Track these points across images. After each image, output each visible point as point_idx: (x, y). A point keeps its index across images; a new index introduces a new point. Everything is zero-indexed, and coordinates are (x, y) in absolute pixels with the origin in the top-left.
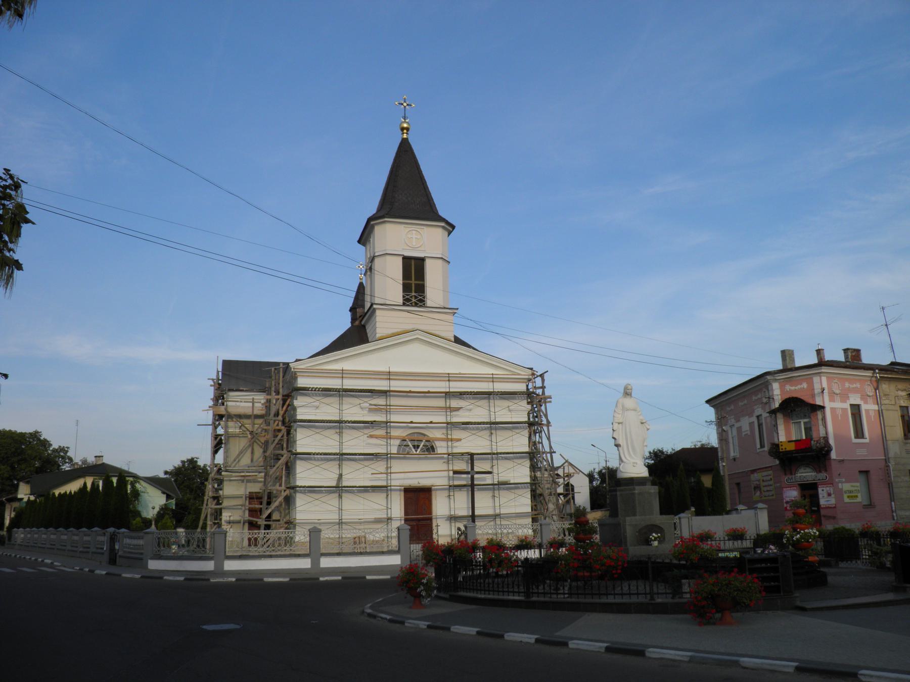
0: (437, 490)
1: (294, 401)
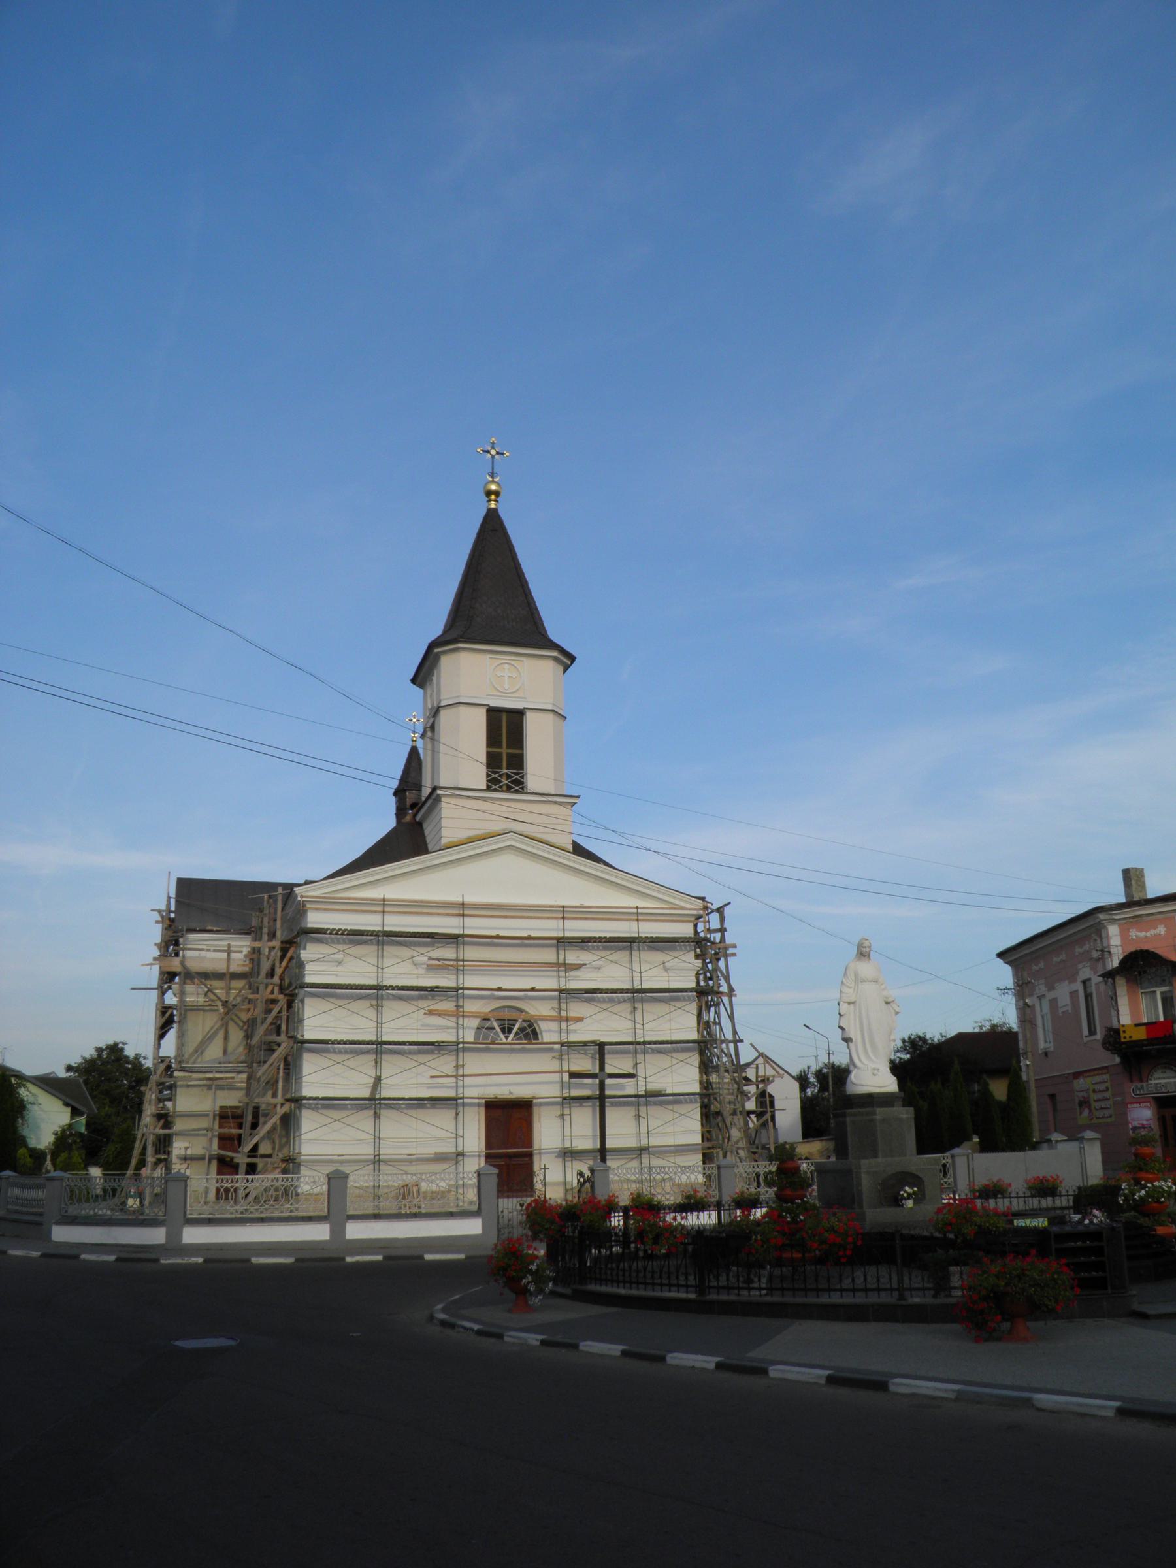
0: (541, 1104)
1: (301, 951)
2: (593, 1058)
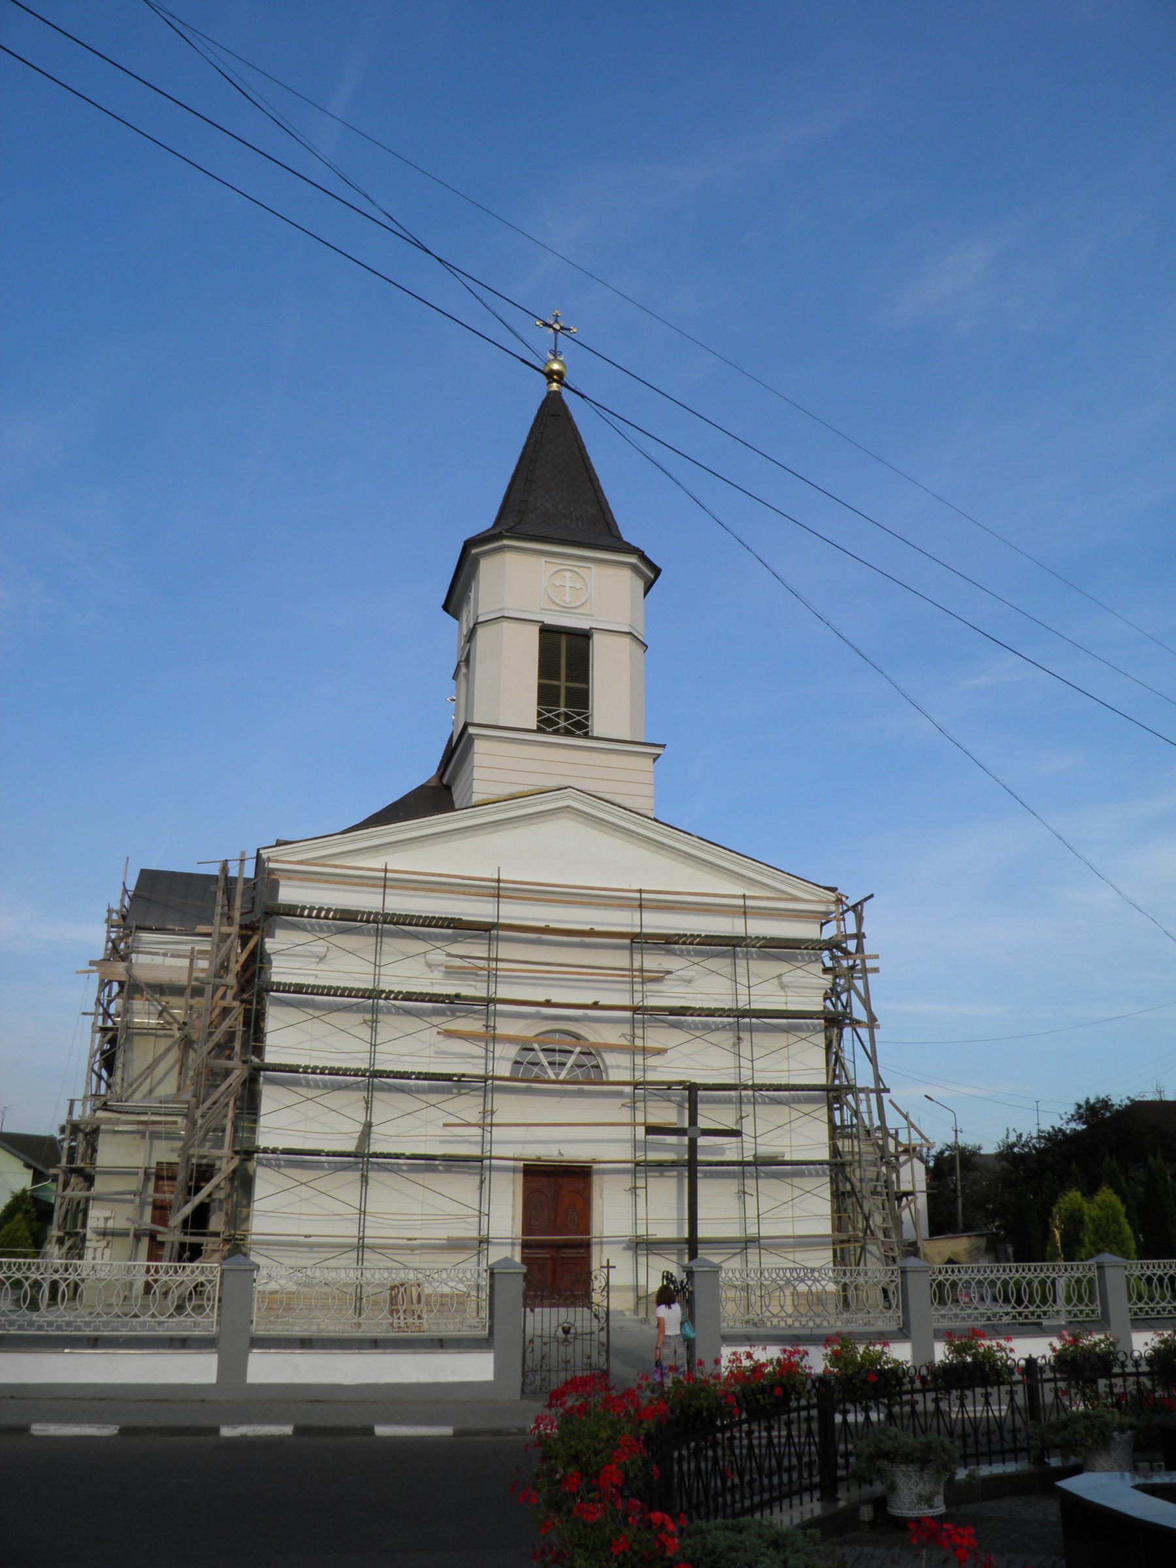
0: (604, 1172)
1: (267, 940)
2: (680, 1106)
